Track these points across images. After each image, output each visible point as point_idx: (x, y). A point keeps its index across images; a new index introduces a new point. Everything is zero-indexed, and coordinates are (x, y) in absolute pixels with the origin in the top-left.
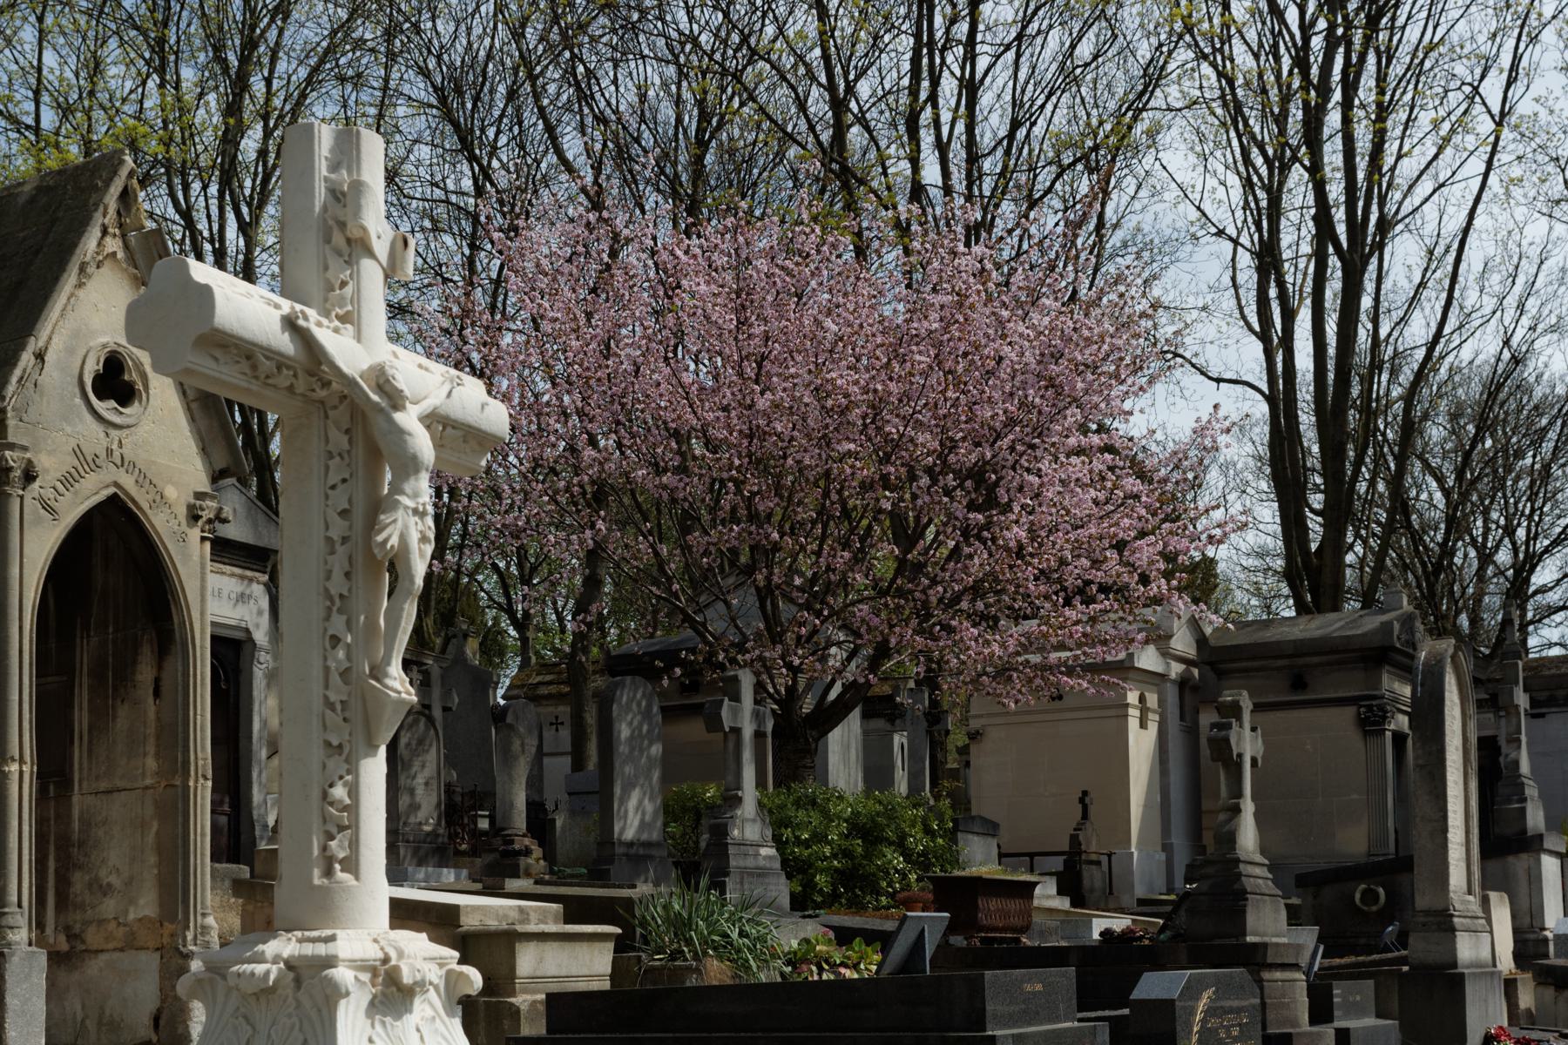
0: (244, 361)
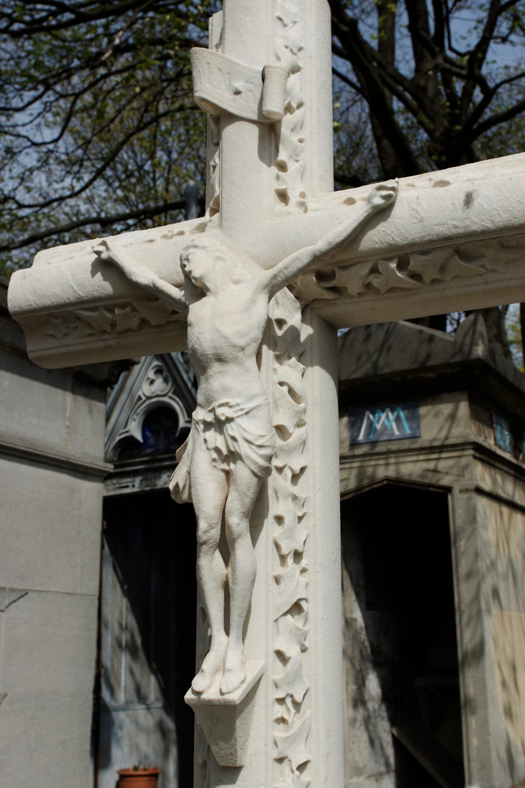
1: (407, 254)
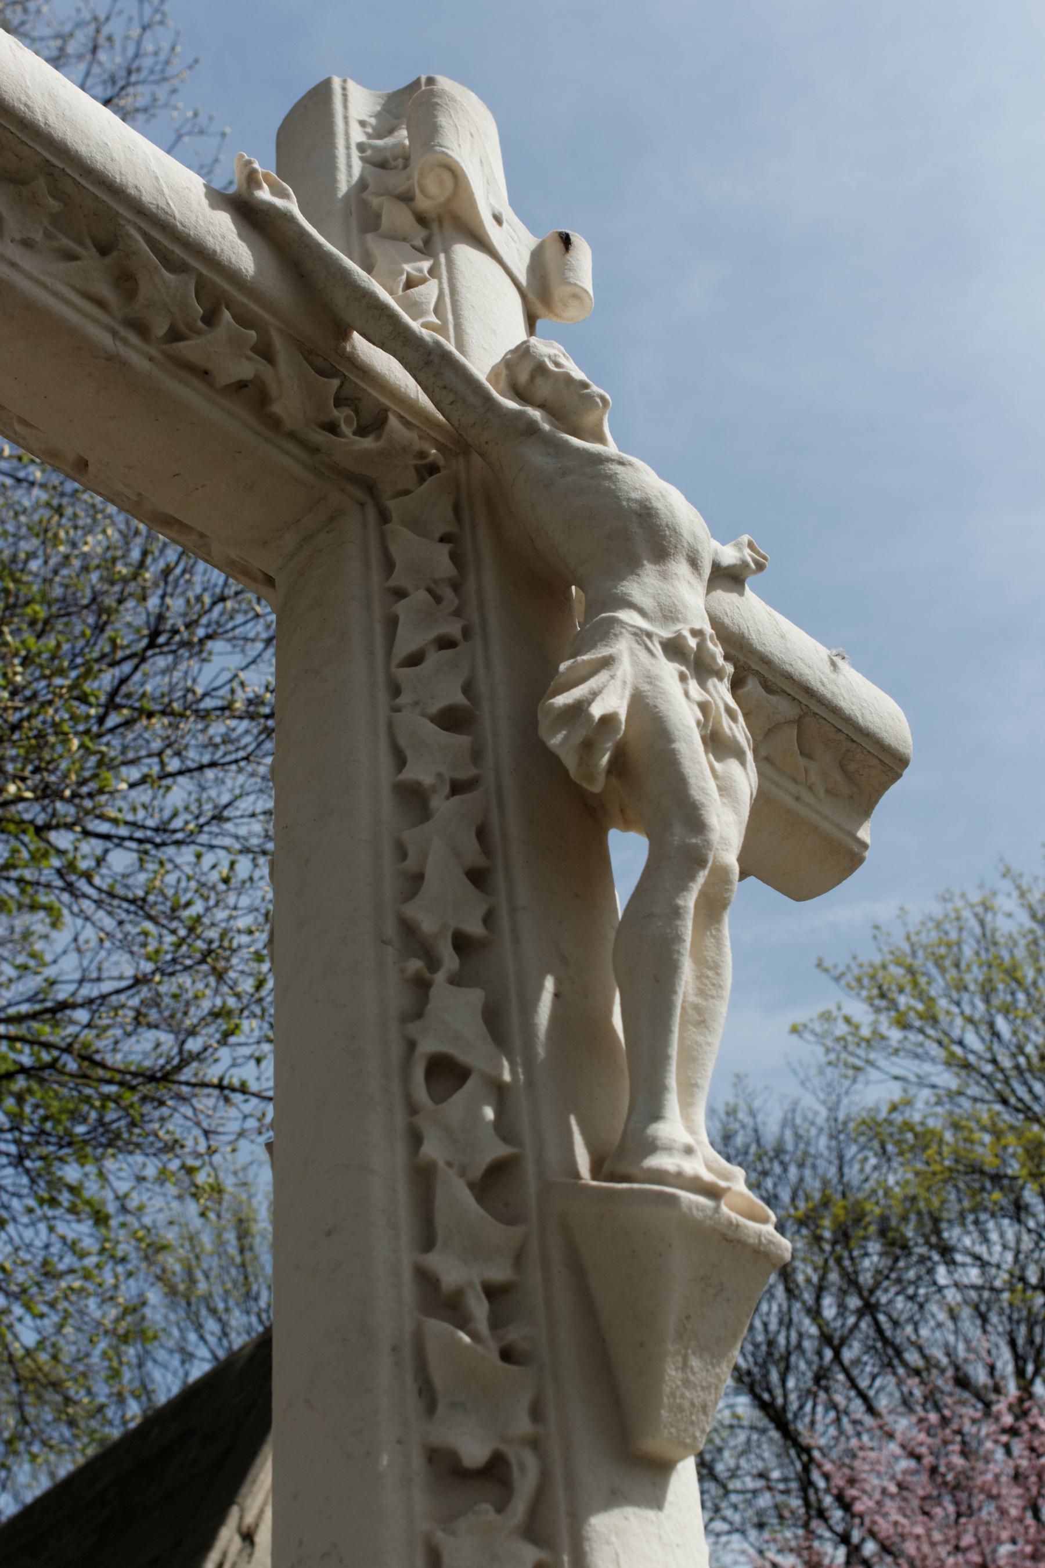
0: (90, 258)
1: (749, 668)
